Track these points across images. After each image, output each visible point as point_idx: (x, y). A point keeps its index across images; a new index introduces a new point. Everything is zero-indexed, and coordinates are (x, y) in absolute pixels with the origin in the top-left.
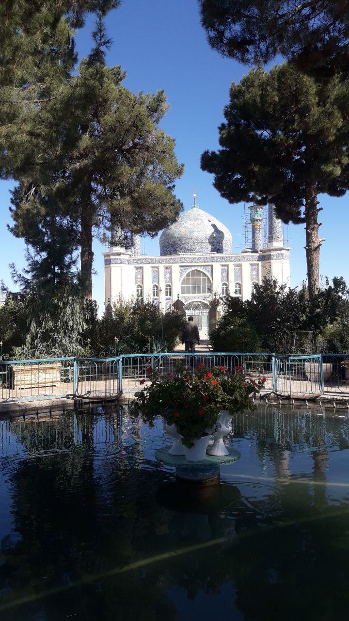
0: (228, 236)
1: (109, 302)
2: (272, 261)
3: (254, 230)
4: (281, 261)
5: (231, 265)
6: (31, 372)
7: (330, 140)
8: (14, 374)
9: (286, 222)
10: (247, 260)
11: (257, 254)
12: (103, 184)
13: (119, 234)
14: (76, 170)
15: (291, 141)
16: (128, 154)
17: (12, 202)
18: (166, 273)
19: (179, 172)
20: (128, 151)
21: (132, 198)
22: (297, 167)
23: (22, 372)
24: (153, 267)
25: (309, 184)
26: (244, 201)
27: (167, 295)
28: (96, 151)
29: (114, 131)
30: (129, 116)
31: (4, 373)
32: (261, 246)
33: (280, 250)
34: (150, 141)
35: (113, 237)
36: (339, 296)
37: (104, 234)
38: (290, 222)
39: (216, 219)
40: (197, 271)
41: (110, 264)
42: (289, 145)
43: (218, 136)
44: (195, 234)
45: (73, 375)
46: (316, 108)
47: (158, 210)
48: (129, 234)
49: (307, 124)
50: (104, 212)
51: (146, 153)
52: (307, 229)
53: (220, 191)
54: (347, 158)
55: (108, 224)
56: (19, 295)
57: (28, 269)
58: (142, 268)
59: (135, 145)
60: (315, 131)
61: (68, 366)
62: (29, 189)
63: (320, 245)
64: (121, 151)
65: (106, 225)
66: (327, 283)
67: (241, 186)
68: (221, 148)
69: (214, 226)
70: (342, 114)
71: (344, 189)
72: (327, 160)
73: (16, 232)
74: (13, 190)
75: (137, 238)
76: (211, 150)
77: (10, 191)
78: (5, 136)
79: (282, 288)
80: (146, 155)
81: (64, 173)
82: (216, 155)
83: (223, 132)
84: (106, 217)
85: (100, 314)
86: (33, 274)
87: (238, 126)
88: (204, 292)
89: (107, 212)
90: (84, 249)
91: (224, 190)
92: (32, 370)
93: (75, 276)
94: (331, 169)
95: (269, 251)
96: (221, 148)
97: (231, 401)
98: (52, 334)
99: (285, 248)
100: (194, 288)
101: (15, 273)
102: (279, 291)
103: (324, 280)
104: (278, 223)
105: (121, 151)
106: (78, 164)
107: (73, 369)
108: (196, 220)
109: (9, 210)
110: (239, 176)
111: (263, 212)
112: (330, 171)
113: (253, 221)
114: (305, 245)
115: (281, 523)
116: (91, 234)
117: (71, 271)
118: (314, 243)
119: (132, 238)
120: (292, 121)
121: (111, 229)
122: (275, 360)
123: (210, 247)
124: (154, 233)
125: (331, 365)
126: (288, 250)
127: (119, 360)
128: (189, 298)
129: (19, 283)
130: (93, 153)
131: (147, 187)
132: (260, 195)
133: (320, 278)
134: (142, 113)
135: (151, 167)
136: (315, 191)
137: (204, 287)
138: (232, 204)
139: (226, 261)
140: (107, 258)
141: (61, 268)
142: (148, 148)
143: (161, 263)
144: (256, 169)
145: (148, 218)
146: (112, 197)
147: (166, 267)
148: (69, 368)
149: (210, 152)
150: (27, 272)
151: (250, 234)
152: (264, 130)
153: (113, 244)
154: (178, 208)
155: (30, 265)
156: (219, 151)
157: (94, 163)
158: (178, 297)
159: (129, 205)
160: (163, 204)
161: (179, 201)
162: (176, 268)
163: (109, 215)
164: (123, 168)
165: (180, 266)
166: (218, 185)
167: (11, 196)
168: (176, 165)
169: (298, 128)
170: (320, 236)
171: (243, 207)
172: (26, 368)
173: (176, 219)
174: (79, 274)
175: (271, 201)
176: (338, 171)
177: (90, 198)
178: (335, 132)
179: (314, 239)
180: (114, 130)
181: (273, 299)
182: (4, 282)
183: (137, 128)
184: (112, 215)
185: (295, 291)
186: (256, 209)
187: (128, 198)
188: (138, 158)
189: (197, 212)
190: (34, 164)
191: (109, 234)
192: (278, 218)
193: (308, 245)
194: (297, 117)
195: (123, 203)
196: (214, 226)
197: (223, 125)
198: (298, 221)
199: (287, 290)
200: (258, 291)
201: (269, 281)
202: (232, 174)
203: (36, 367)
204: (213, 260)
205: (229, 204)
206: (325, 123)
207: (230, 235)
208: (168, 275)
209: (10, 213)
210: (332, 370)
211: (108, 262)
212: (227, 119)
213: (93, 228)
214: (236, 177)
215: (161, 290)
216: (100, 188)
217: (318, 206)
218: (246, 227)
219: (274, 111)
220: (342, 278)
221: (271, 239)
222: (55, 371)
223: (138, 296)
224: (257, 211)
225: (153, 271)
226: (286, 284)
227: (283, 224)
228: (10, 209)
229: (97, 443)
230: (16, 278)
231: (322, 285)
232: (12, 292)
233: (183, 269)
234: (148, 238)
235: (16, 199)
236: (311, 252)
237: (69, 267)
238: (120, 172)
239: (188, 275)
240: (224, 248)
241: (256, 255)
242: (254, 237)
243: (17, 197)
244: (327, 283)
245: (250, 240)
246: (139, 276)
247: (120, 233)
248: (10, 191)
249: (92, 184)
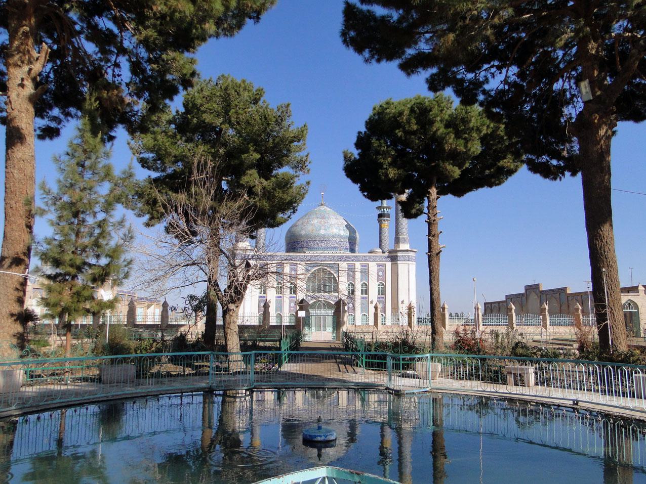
2: (398, 262)
4: (407, 262)
5: (358, 265)
27: (362, 294)
33: (407, 251)
44: (322, 232)
108: (323, 218)
115: (38, 322)
139: (352, 261)
221: (397, 241)
229: (373, 338)
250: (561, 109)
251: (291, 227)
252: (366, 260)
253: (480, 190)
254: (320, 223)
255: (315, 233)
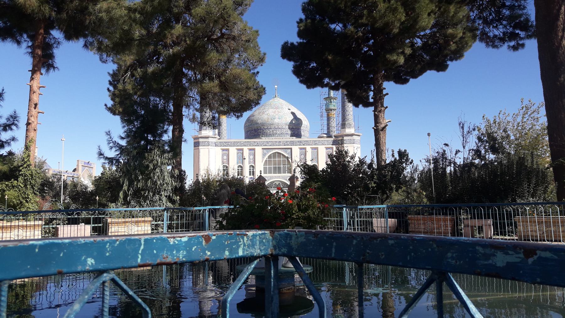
0: (305, 123)
1: (197, 177)
3: (329, 119)
5: (308, 148)
6: (124, 224)
7: (394, 32)
8: (109, 226)
9: (356, 105)
10: (323, 144)
11: (332, 139)
12: (193, 69)
13: (207, 115)
14: (170, 56)
15: (361, 34)
16: (216, 43)
17: (110, 83)
18: (250, 154)
19: (261, 60)
20: (216, 40)
21: (220, 81)
22: (365, 59)
23: (116, 225)
24: (238, 150)
25: (376, 73)
26: (320, 87)
27: (250, 175)
28: (187, 39)
29: (204, 21)
30: (217, 9)
31: (99, 225)
32: (334, 132)
33: (352, 135)
34: (236, 32)
35: (202, 117)
36: (403, 167)
37: (194, 115)
38: (360, 106)
39: (295, 108)
40: (278, 153)
41: (199, 146)
42: (359, 38)
43: (296, 30)
44: (276, 121)
45: (163, 229)
46: (382, 4)
47: (243, 93)
48: (217, 115)
49: (374, 18)
50: (194, 94)
51: (232, 42)
52: (374, 111)
53: (298, 77)
54: (410, 49)
55: (198, 106)
56: (115, 159)
57: (123, 136)
58: (228, 150)
59: (223, 35)
60: (382, 25)
61: (159, 221)
62: (126, 72)
63: (386, 125)
64: (210, 40)
65: (196, 107)
66: (393, 156)
67: (317, 73)
68: (299, 40)
69: (293, 114)
70: (405, 10)
71: (408, 78)
72: (392, 51)
73: (112, 110)
74: (111, 72)
75: (224, 118)
76: (290, 41)
77: (109, 73)
78: (105, 11)
79: (352, 157)
80: (233, 44)
81: (158, 59)
82: (295, 45)
83: (301, 25)
84: (196, 100)
85: (189, 182)
86: (128, 140)
87: (313, 20)
88: (284, 172)
89: (197, 94)
90: (175, 127)
91: (302, 77)
92: (125, 222)
93: (166, 143)
94: (395, 58)
95: (343, 136)
96: (299, 40)
97: (304, 218)
98: (143, 193)
99: (356, 134)
100: (275, 168)
101: (110, 140)
102: (349, 160)
103: (391, 153)
104: (350, 106)
105: (210, 40)
106: (171, 50)
107: (163, 224)
108: (277, 108)
109: (107, 91)
110: (315, 65)
111: (337, 95)
112: (394, 60)
113: (328, 110)
114: (373, 125)
116: (182, 113)
117: (163, 139)
118: (381, 124)
119: (219, 119)
120: (361, 16)
121: (201, 110)
122: (346, 210)
123: (289, 132)
124: (239, 114)
125: (396, 220)
126: (359, 136)
127: (206, 209)
128: (271, 178)
129: (114, 149)
130: (185, 41)
131: (234, 72)
132: (333, 81)
133: (386, 151)
134: (228, 6)
135: (237, 56)
136: (381, 79)
137: (284, 168)
138: (309, 90)
140: (196, 141)
141: (154, 136)
142: (234, 38)
143: (245, 146)
144: (330, 58)
145: (234, 101)
146: (201, 81)
147: (250, 150)
148: (159, 223)
149: (289, 42)
150: (122, 138)
151: (325, 122)
152: (337, 25)
153: (202, 124)
154: (260, 92)
155: (125, 132)
156: (297, 43)
157: (186, 50)
158: (261, 173)
159: (218, 87)
160: (247, 88)
161: (262, 86)
162: (259, 150)
163: (198, 98)
164: (212, 54)
165: (263, 149)
166: (297, 72)
167: (109, 78)
168: (259, 53)
169: (367, 22)
170: (387, 117)
171: (320, 92)
172: (120, 221)
173: (259, 102)
174: (170, 141)
175: (343, 87)
176: (402, 60)
177: (181, 81)
178: (398, 25)
179: (381, 120)
180: (204, 21)
181: (345, 167)
182: (101, 148)
183: (225, 20)
184: (202, 98)
185: (364, 160)
186: (331, 100)
187: (216, 82)
188: (225, 47)
189: (278, 101)
190: (133, 39)
191: (198, 115)
192: (349, 102)
193: (376, 126)
194: (365, 12)
195: (212, 85)
196: (293, 114)
197: (301, 20)
198: (367, 104)
199: (357, 159)
200: (332, 160)
201: (342, 151)
202: (308, 63)
203: (129, 220)
204: (293, 143)
205: (306, 89)
206: (390, 17)
207: (308, 122)
208: (252, 157)
209: (108, 93)
210: (397, 224)
211: (197, 144)
212: (304, 14)
213: (184, 109)
214: (312, 65)
215: (245, 159)
216: (190, 73)
217: (385, 92)
218: (322, 116)
219: (345, 7)
220: (405, 151)
221: (343, 126)
222: (146, 225)
223: (224, 170)
224: (331, 102)
225: (238, 153)
226: (356, 154)
227: (354, 107)
228: (108, 89)
230: (111, 145)
231: (388, 158)
232: (109, 157)
233: (265, 151)
234: (234, 118)
235: (113, 81)
236: (378, 132)
237: (161, 135)
238: (209, 58)
239: (270, 157)
240: (302, 133)
241: (331, 139)
242: (328, 125)
243: (115, 79)
244: (393, 156)
245: (326, 128)
246: (225, 157)
247: (208, 114)
248: (109, 73)
249: (184, 70)
250: (294, 69)
251: (249, 118)
252: (315, 144)
253: (425, 74)
254: (275, 112)
255: (270, 122)
